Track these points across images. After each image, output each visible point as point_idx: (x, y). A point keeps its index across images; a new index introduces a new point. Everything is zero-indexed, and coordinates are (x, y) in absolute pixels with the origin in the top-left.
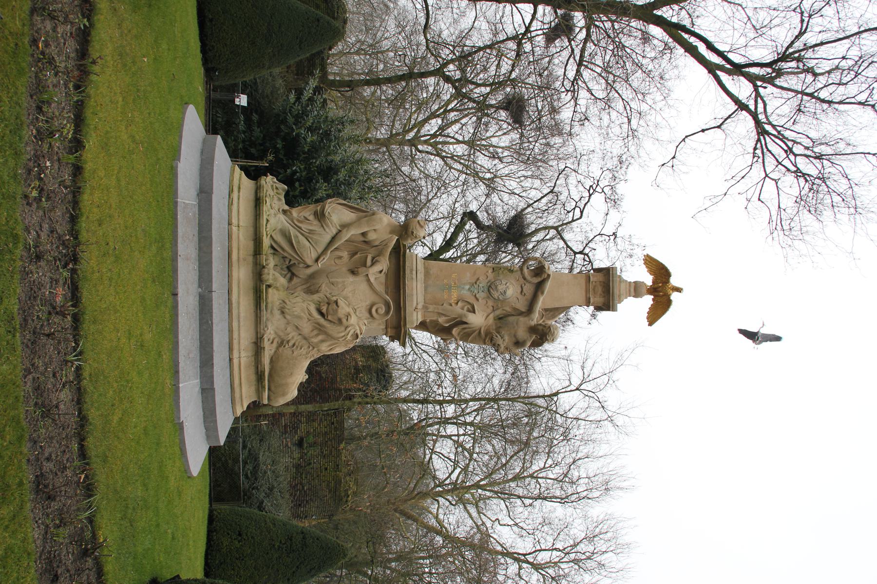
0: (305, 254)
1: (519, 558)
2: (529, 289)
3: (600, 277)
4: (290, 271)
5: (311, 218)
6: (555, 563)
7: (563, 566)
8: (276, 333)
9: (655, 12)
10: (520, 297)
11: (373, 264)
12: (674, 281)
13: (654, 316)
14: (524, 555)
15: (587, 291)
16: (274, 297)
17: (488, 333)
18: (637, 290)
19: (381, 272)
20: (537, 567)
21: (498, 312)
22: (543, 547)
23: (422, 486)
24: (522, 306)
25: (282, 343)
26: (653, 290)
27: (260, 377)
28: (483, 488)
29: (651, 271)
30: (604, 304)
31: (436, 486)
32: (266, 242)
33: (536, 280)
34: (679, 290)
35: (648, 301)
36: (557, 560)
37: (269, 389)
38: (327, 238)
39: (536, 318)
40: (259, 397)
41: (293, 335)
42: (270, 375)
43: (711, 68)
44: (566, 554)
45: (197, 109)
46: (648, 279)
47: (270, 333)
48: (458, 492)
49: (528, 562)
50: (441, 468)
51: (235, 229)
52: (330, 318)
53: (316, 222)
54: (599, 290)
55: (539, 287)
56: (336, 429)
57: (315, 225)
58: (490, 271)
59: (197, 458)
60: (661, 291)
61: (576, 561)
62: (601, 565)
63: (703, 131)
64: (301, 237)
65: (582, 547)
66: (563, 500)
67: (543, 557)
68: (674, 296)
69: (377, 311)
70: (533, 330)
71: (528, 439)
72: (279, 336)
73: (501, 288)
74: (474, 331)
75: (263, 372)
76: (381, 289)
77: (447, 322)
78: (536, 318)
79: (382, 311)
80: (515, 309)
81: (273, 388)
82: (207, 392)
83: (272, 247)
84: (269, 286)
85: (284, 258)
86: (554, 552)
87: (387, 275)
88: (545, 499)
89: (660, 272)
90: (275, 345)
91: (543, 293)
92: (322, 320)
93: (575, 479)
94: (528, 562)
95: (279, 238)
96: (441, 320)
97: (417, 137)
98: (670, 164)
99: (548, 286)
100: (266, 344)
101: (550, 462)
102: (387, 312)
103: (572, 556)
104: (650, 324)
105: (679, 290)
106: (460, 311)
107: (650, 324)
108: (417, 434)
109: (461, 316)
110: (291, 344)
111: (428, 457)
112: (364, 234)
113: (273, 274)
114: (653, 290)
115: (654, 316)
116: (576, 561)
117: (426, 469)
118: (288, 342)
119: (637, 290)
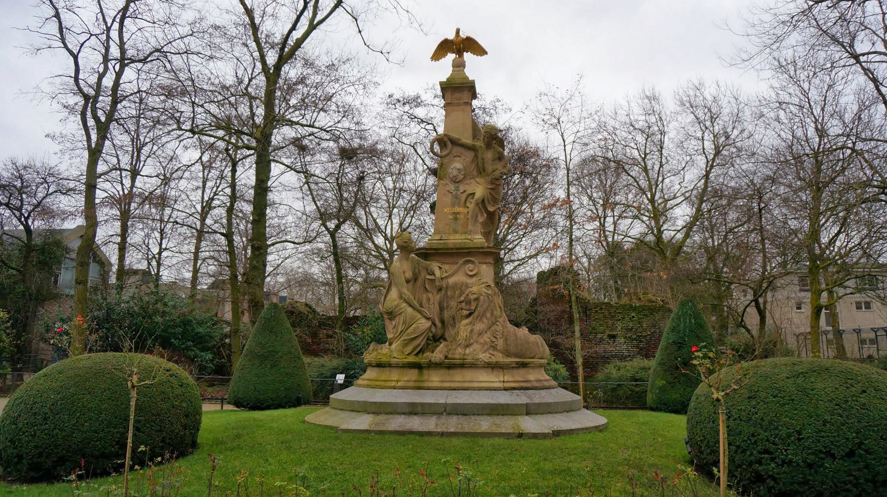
0: (421, 328)
1: (710, 167)
2: (457, 150)
3: (448, 94)
4: (436, 339)
5: (394, 323)
6: (714, 136)
7: (716, 131)
8: (485, 352)
9: (271, 71)
10: (463, 157)
11: (434, 274)
12: (451, 36)
13: (480, 51)
14: (708, 162)
15: (458, 105)
16: (458, 353)
17: (492, 183)
18: (459, 65)
19: (440, 268)
20: (718, 153)
21: (475, 173)
22: (701, 147)
23: (657, 248)
24: (470, 155)
25: (493, 347)
26: (460, 52)
27: (524, 365)
28: (653, 196)
29: (444, 55)
30: (470, 91)
31: (652, 233)
32: (412, 359)
33: (449, 144)
34: (458, 31)
35: (468, 56)
36: (712, 135)
37: (533, 358)
38: (410, 310)
39: (479, 144)
40: (541, 367)
41: (486, 338)
42: (520, 357)
43: (312, 27)
44: (706, 128)
45: (310, 413)
46: (451, 57)
47: (484, 357)
48: (659, 214)
49: (713, 160)
50: (637, 229)
51: (400, 384)
52: (473, 308)
53: (397, 319)
54: (457, 95)
55: (455, 143)
56: (601, 309)
57: (400, 320)
58: (442, 182)
59: (593, 418)
60: (460, 46)
61: (713, 119)
62: (715, 99)
63: (360, 32)
64: (408, 331)
65: (701, 115)
66: (663, 133)
67: (709, 146)
68: (463, 35)
69: (471, 271)
70: (488, 146)
71: (614, 162)
72: (488, 349)
73: (455, 173)
74: (491, 194)
75: (517, 363)
76: (455, 267)
77: (482, 214)
78: (479, 144)
79: (471, 266)
80: (472, 161)
81: (532, 355)
82: (529, 410)
83: (417, 354)
84: (446, 357)
85: (428, 344)
86: (705, 138)
87: (443, 263)
88: (662, 148)
89: (445, 47)
90: (495, 353)
91: (460, 140)
92: (476, 313)
93: (646, 125)
94: (713, 160)
95: (409, 349)
96: (481, 219)
97: (387, 251)
98: (386, 55)
99: (455, 135)
100: (494, 360)
101: (632, 145)
102: (472, 262)
103: (708, 124)
104: (486, 53)
105: (458, 31)
106: (473, 205)
107: (486, 53)
108: (614, 250)
109: (477, 204)
110: (494, 340)
111: (630, 239)
112: (408, 281)
113: (437, 355)
114: (460, 52)
115: (480, 51)
116: (713, 119)
117: (640, 242)
118: (493, 342)
119: (459, 65)
